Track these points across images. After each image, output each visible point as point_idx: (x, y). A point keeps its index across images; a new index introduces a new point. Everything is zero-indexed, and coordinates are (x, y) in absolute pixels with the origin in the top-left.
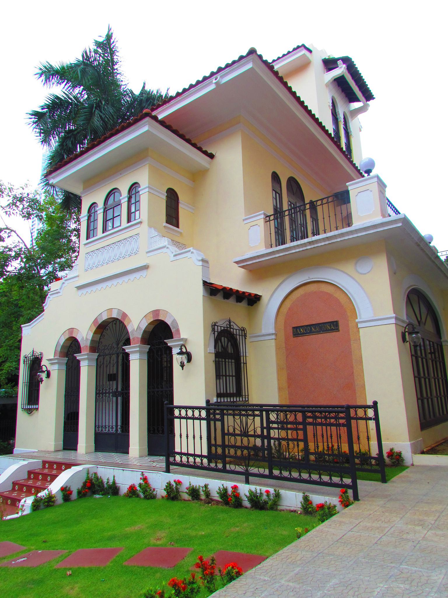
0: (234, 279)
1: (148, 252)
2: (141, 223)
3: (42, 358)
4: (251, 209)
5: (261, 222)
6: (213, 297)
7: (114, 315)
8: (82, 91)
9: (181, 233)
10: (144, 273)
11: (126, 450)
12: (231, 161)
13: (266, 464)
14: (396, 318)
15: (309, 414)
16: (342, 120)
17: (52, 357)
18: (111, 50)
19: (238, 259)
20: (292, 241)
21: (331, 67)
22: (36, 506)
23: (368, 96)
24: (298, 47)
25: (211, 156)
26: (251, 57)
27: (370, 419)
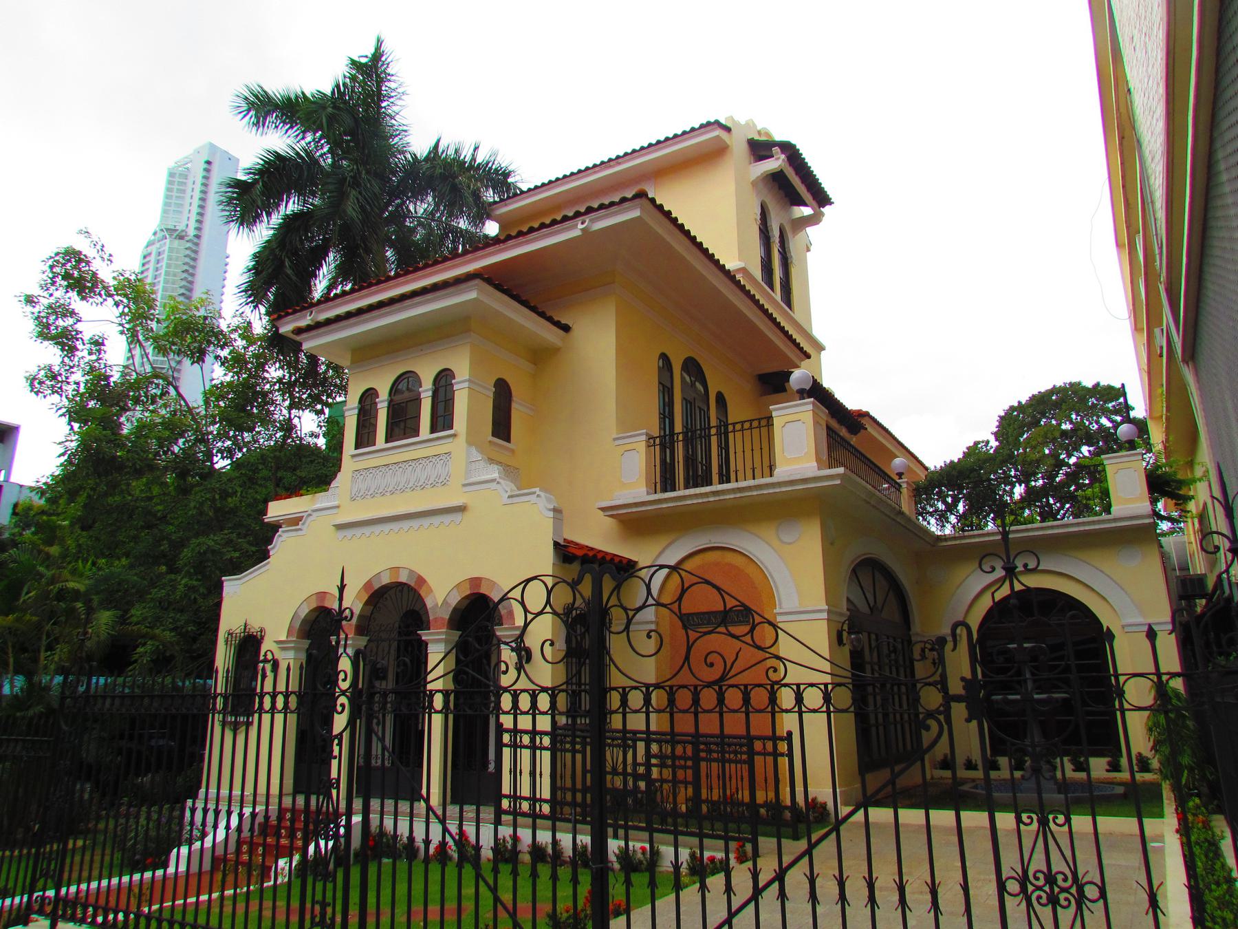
0: (598, 535)
1: (464, 485)
2: (454, 435)
3: (262, 638)
4: (626, 425)
5: (643, 444)
6: (567, 565)
7: (403, 578)
8: (320, 140)
9: (512, 451)
10: (457, 517)
11: (413, 792)
12: (599, 345)
13: (643, 816)
14: (829, 612)
15: (702, 747)
16: (777, 240)
17: (284, 638)
18: (378, 76)
19: (604, 504)
20: (686, 487)
21: (763, 153)
22: (304, 870)
23: (822, 199)
24: (709, 124)
25: (566, 329)
26: (637, 201)
27: (782, 755)
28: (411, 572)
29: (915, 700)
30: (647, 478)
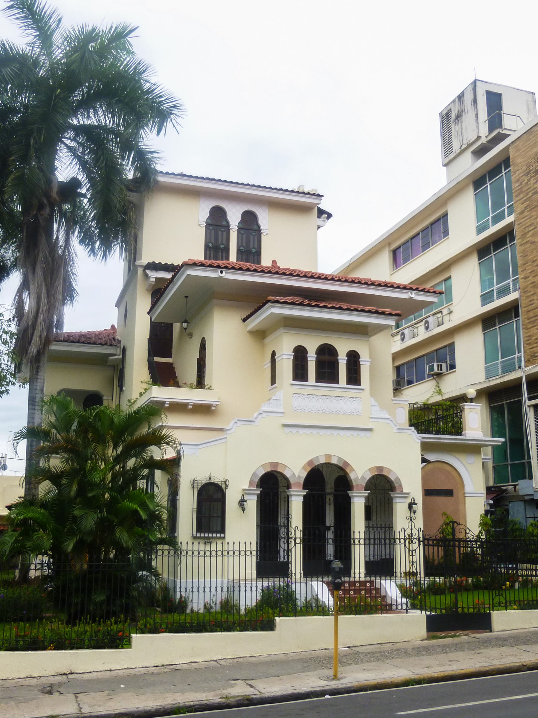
28: (370, 470)
29: (482, 551)
30: (257, 526)
